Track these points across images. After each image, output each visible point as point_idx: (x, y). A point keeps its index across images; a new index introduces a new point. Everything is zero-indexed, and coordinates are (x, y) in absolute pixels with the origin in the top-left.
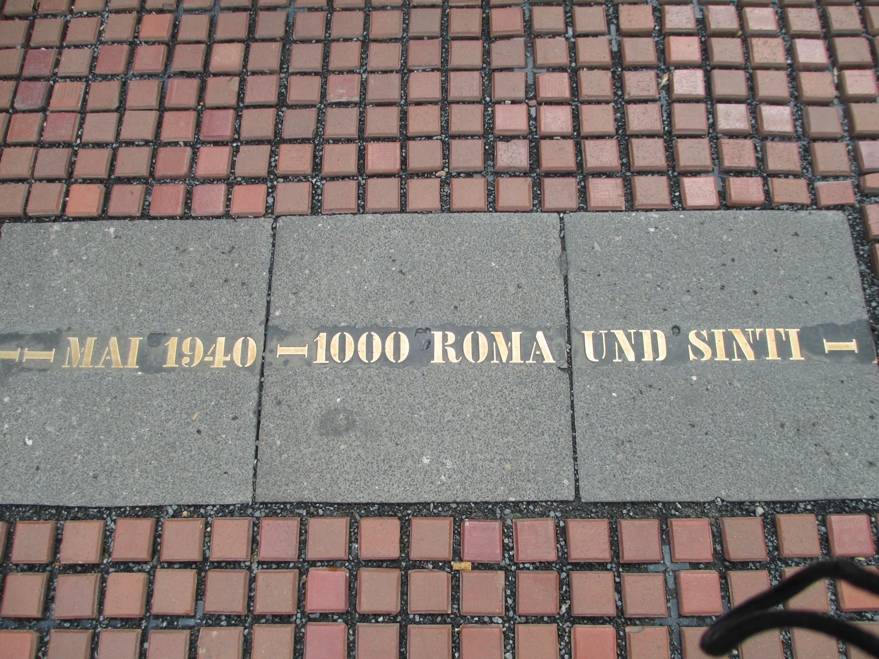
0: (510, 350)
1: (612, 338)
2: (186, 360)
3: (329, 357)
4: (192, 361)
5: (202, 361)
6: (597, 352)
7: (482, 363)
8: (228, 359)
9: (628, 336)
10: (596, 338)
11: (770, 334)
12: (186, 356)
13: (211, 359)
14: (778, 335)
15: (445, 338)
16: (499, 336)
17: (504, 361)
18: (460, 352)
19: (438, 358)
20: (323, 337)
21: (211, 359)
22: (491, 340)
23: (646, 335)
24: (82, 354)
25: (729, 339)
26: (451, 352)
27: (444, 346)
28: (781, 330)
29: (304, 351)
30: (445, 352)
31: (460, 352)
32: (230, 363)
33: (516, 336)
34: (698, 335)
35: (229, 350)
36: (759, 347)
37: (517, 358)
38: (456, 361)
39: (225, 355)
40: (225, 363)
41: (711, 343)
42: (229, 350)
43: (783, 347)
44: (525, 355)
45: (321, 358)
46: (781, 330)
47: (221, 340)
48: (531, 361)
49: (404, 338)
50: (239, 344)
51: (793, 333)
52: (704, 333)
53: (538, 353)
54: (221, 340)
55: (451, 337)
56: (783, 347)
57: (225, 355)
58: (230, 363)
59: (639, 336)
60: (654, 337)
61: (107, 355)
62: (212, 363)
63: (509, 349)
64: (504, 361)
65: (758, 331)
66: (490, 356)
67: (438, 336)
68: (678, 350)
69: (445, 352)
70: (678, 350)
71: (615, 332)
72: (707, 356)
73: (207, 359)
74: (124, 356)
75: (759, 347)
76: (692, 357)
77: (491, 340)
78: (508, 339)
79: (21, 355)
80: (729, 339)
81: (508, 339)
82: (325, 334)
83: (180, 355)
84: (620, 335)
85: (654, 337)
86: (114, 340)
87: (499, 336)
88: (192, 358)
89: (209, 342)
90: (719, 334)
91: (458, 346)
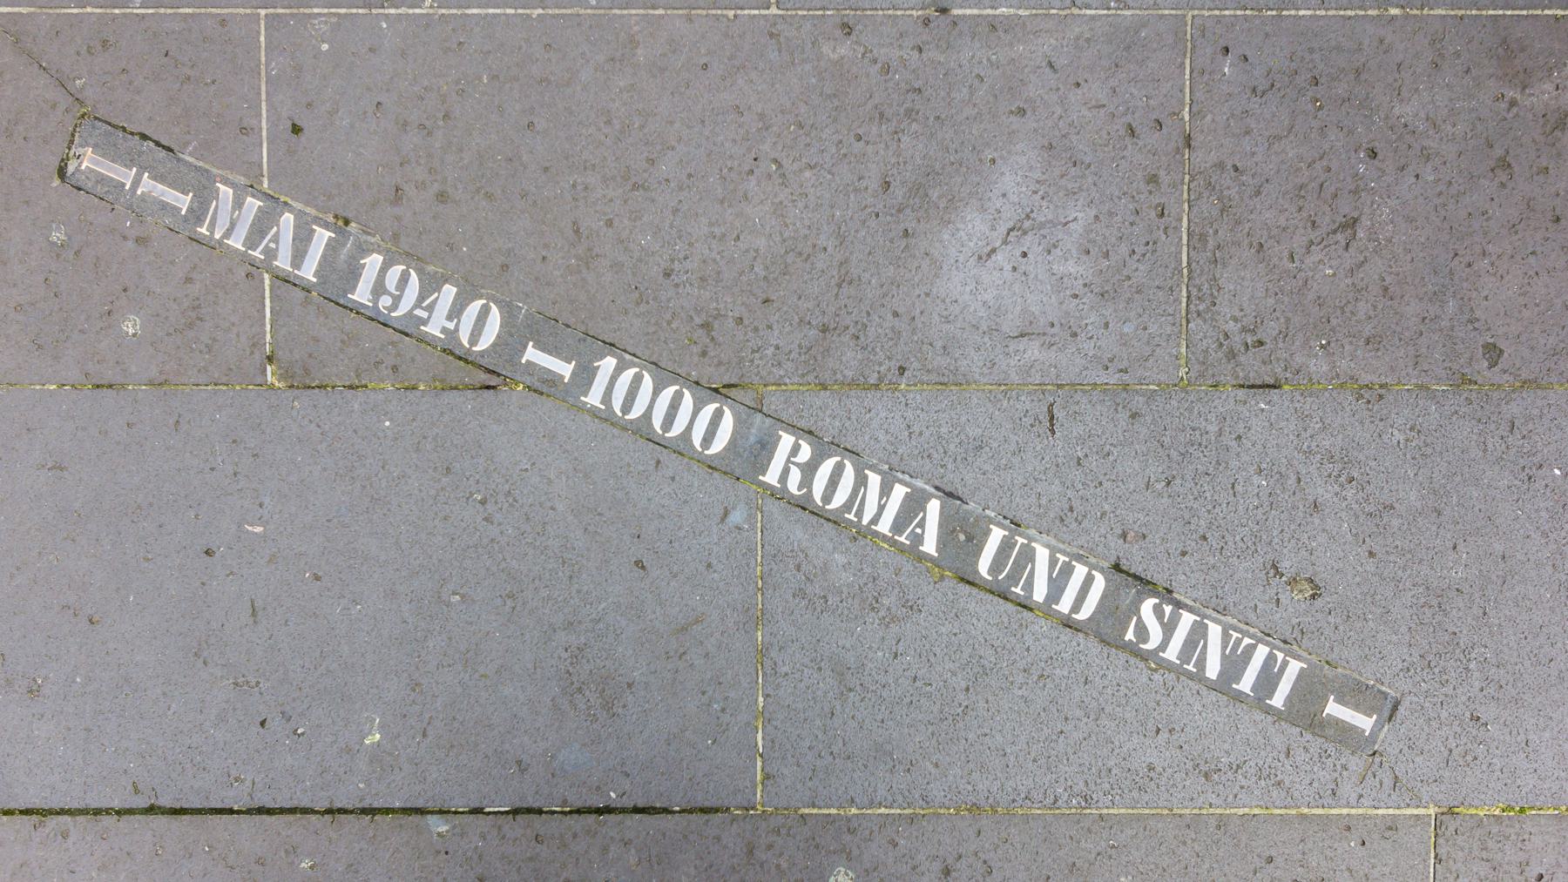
0: (881, 508)
1: (1028, 556)
2: (385, 301)
3: (607, 397)
4: (395, 307)
5: (410, 314)
6: (996, 567)
7: (631, 421)
8: (451, 326)
9: (1053, 562)
10: (1006, 547)
11: (1262, 652)
12: (390, 294)
13: (424, 315)
14: (1271, 658)
15: (795, 450)
16: (874, 480)
17: (865, 522)
18: (807, 481)
19: (771, 477)
20: (609, 363)
21: (424, 315)
22: (861, 481)
23: (1080, 571)
24: (881, 508)
25: (1198, 632)
26: (795, 476)
27: (788, 461)
28: (1280, 656)
29: (565, 369)
30: (786, 471)
31: (807, 481)
32: (452, 334)
33: (899, 492)
34: (1158, 611)
35: (456, 312)
36: (1234, 664)
37: (884, 527)
38: (796, 492)
39: (449, 318)
40: (444, 330)
41: (1169, 628)
42: (456, 312)
43: (1268, 680)
44: (898, 526)
45: (594, 398)
46: (1280, 656)
47: (449, 291)
48: (902, 539)
49: (495, 315)
50: (827, 467)
51: (1295, 667)
52: (1168, 609)
53: (919, 531)
54: (449, 291)
55: (805, 453)
56: (1268, 680)
57: (449, 318)
58: (452, 334)
59: (1067, 571)
60: (1089, 580)
61: (917, 526)
62: (425, 322)
63: (881, 506)
64: (865, 522)
65: (1247, 641)
66: (847, 506)
67: (787, 440)
68: (340, 272)
69: (786, 471)
70: (340, 272)
71: (1211, 625)
72: (1151, 645)
73: (418, 312)
74: (298, 257)
75: (1234, 664)
76: (1130, 635)
77: (861, 481)
78: (886, 491)
79: (136, 182)
80: (1198, 632)
81: (886, 491)
82: (614, 361)
83: (379, 289)
84: (1042, 554)
85: (1089, 580)
86: (288, 219)
87: (874, 480)
88: (397, 300)
89: (430, 286)
90: (1187, 619)
91: (809, 469)
